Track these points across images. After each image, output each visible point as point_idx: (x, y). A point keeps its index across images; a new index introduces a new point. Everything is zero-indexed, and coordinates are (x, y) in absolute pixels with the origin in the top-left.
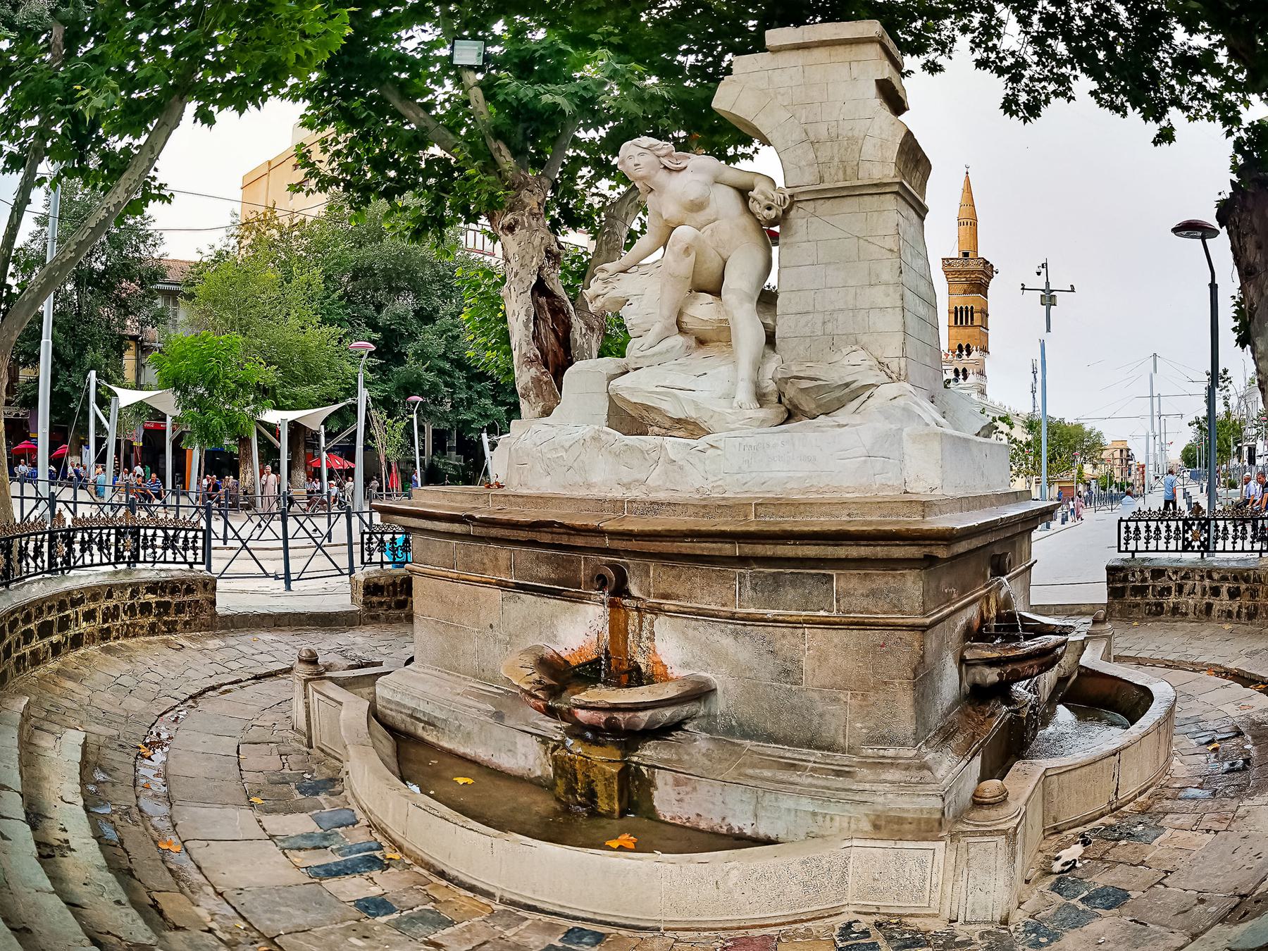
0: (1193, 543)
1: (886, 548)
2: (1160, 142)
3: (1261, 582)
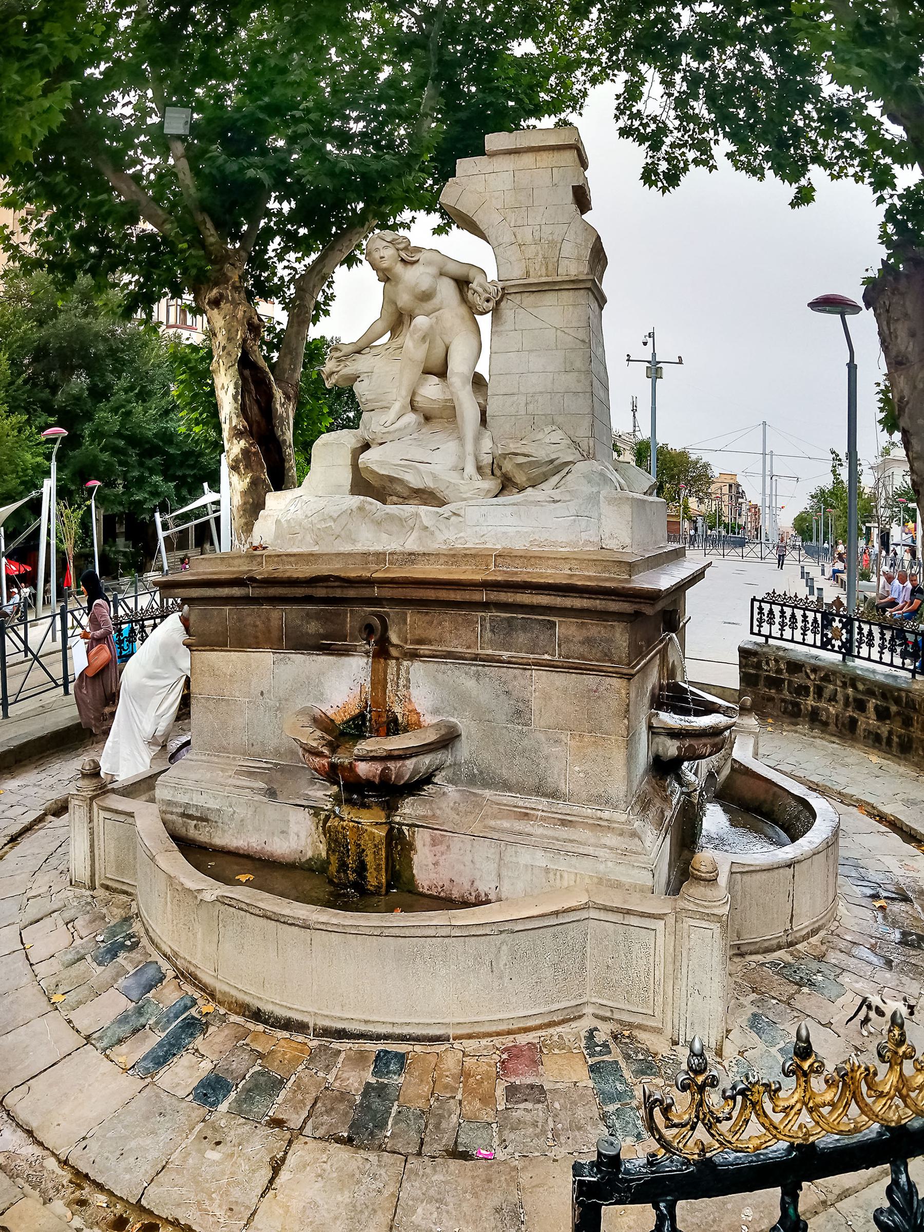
0: (840, 626)
1: (604, 602)
2: (798, 205)
3: (915, 709)
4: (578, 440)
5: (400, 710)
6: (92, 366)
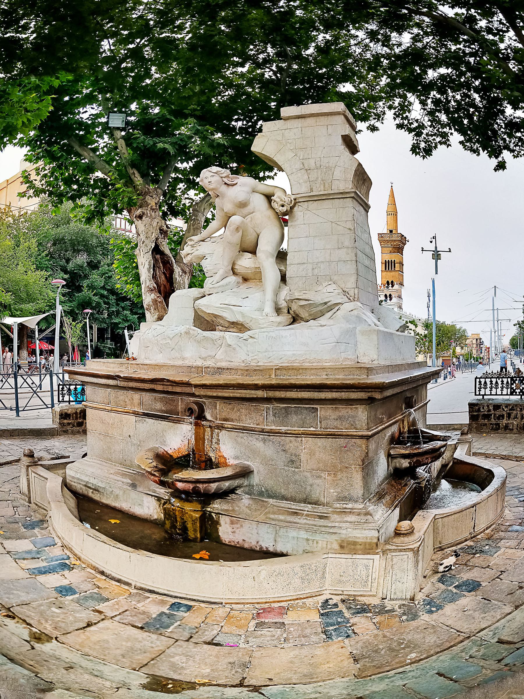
4: (347, 290)
5: (213, 455)
6: (89, 250)
